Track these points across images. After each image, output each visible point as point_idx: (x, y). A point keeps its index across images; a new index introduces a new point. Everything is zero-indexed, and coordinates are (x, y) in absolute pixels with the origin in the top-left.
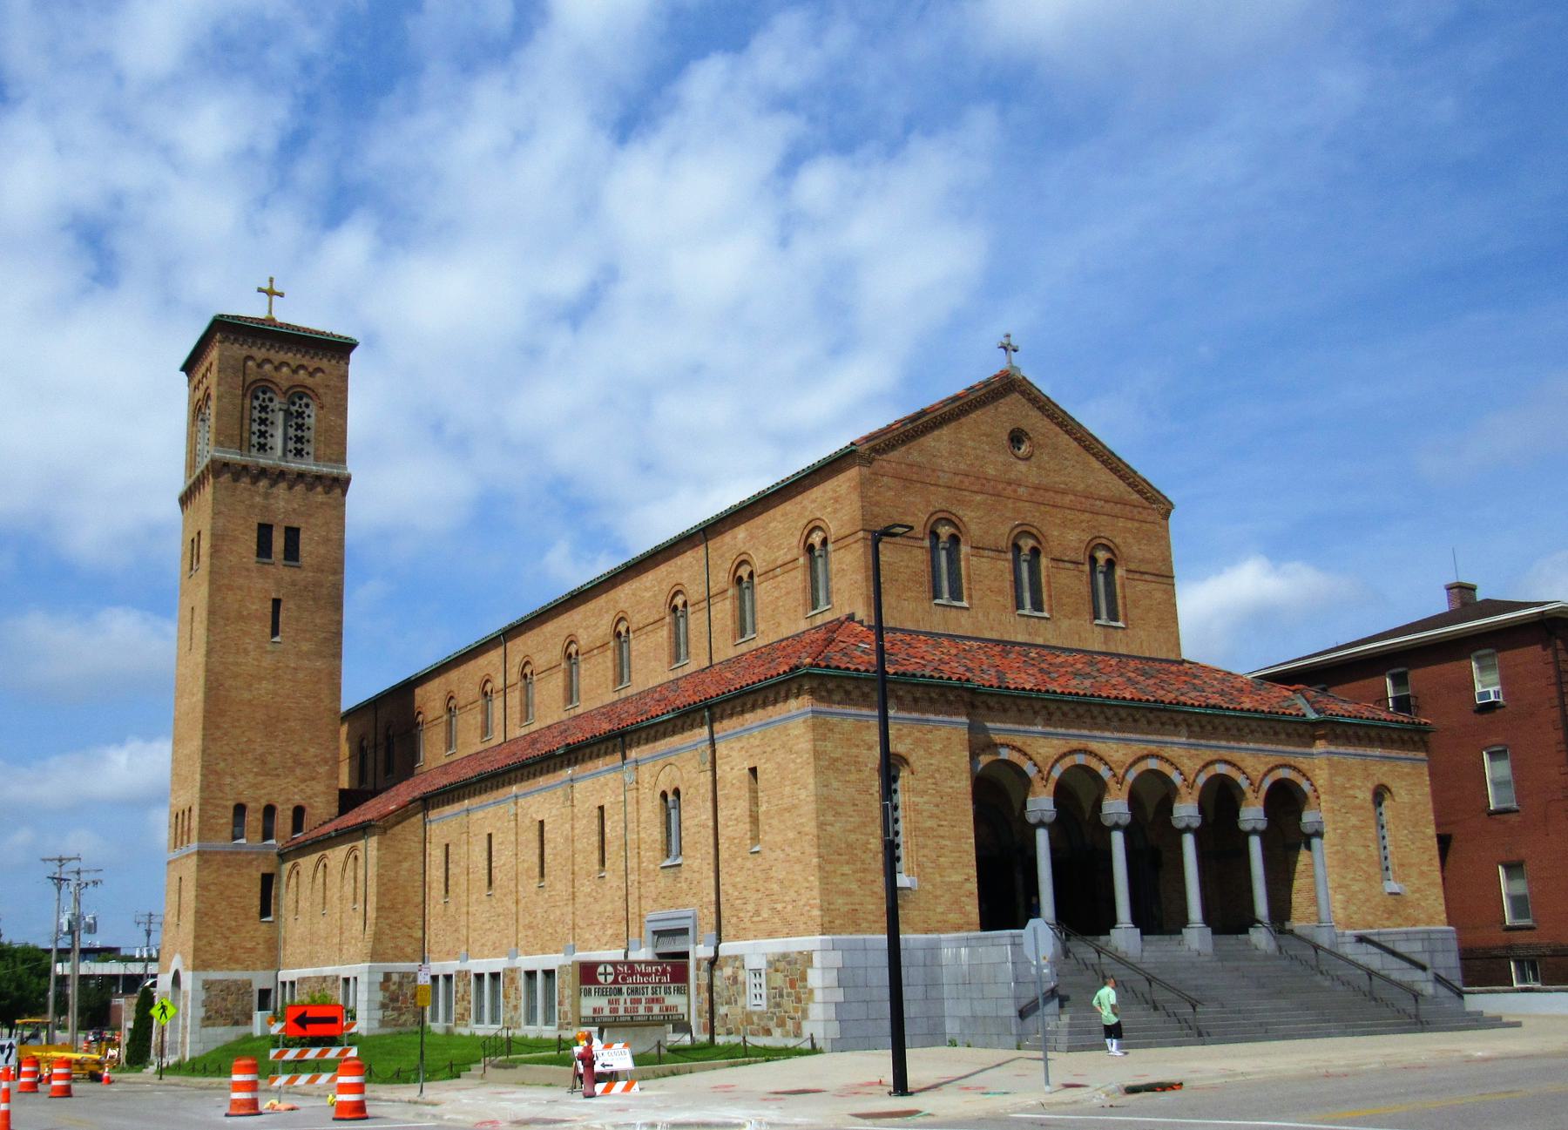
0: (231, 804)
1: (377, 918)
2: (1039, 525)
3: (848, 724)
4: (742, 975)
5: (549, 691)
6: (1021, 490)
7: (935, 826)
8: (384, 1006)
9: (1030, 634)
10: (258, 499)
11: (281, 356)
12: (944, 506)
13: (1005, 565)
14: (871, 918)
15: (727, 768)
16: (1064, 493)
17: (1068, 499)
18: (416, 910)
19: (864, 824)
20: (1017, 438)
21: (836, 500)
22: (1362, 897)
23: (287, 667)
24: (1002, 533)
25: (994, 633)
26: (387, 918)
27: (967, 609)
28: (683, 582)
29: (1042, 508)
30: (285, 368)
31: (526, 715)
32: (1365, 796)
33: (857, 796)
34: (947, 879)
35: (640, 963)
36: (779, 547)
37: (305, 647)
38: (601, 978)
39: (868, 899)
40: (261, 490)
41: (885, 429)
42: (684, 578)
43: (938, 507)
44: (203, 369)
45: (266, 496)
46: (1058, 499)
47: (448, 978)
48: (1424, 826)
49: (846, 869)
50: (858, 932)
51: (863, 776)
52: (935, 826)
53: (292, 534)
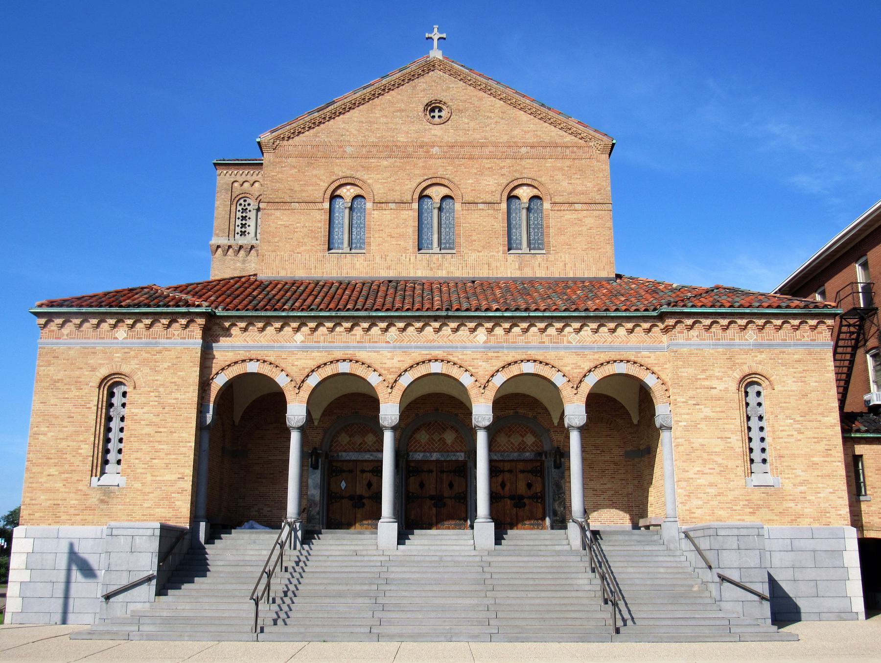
2: (450, 177)
6: (435, 150)
7: (153, 433)
9: (431, 269)
10: (238, 264)
12: (348, 173)
13: (410, 215)
14: (72, 511)
16: (482, 146)
17: (487, 151)
19: (77, 433)
22: (712, 491)
24: (409, 187)
25: (391, 272)
29: (457, 162)
32: (728, 385)
33: (73, 410)
34: (159, 478)
39: (72, 495)
40: (241, 259)
43: (341, 174)
46: (476, 152)
48: (822, 414)
49: (53, 471)
51: (83, 392)
52: (153, 433)
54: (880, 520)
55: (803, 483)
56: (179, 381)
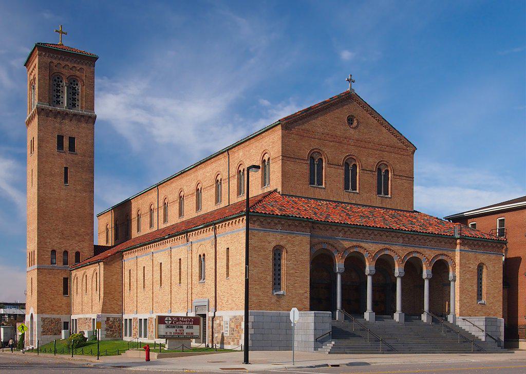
0: (50, 250)
1: (104, 296)
3: (261, 234)
4: (222, 323)
5: (173, 210)
8: (107, 330)
11: (63, 63)
13: (341, 171)
15: (220, 247)
17: (370, 145)
18: (119, 294)
20: (350, 120)
21: (273, 143)
23: (71, 195)
24: (341, 158)
26: (108, 297)
27: (324, 188)
28: (221, 170)
30: (66, 69)
31: (165, 220)
35: (181, 317)
36: (254, 160)
37: (79, 187)
38: (166, 322)
41: (294, 114)
42: (221, 169)
44: (33, 66)
45: (61, 123)
47: (130, 320)
49: (257, 287)
50: (261, 309)
53: (72, 140)
54: (525, 320)
55: (492, 303)
56: (303, 251)
